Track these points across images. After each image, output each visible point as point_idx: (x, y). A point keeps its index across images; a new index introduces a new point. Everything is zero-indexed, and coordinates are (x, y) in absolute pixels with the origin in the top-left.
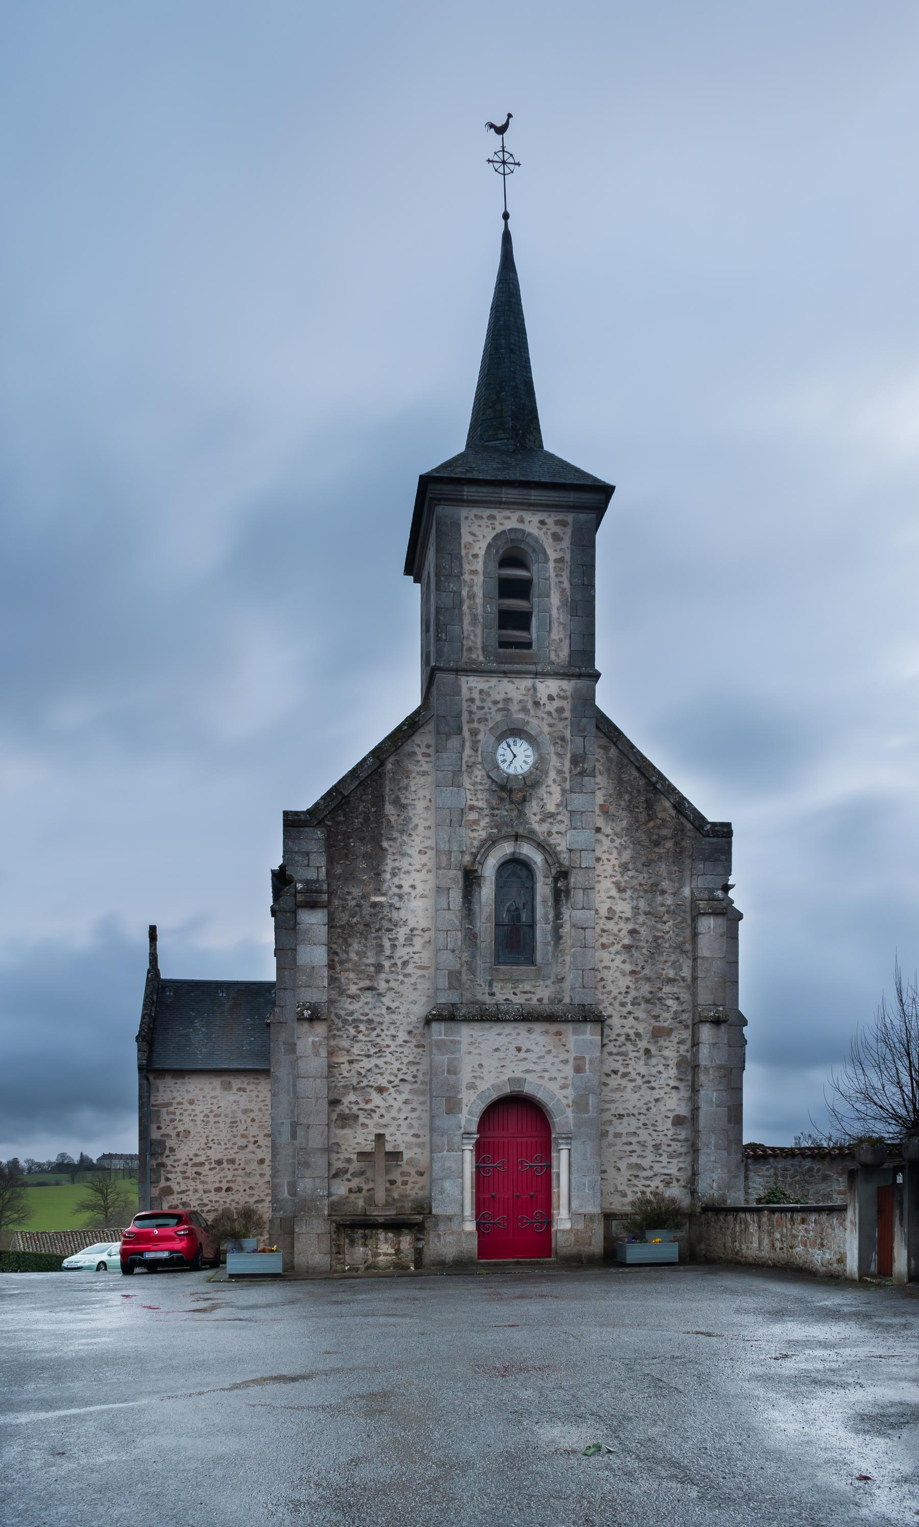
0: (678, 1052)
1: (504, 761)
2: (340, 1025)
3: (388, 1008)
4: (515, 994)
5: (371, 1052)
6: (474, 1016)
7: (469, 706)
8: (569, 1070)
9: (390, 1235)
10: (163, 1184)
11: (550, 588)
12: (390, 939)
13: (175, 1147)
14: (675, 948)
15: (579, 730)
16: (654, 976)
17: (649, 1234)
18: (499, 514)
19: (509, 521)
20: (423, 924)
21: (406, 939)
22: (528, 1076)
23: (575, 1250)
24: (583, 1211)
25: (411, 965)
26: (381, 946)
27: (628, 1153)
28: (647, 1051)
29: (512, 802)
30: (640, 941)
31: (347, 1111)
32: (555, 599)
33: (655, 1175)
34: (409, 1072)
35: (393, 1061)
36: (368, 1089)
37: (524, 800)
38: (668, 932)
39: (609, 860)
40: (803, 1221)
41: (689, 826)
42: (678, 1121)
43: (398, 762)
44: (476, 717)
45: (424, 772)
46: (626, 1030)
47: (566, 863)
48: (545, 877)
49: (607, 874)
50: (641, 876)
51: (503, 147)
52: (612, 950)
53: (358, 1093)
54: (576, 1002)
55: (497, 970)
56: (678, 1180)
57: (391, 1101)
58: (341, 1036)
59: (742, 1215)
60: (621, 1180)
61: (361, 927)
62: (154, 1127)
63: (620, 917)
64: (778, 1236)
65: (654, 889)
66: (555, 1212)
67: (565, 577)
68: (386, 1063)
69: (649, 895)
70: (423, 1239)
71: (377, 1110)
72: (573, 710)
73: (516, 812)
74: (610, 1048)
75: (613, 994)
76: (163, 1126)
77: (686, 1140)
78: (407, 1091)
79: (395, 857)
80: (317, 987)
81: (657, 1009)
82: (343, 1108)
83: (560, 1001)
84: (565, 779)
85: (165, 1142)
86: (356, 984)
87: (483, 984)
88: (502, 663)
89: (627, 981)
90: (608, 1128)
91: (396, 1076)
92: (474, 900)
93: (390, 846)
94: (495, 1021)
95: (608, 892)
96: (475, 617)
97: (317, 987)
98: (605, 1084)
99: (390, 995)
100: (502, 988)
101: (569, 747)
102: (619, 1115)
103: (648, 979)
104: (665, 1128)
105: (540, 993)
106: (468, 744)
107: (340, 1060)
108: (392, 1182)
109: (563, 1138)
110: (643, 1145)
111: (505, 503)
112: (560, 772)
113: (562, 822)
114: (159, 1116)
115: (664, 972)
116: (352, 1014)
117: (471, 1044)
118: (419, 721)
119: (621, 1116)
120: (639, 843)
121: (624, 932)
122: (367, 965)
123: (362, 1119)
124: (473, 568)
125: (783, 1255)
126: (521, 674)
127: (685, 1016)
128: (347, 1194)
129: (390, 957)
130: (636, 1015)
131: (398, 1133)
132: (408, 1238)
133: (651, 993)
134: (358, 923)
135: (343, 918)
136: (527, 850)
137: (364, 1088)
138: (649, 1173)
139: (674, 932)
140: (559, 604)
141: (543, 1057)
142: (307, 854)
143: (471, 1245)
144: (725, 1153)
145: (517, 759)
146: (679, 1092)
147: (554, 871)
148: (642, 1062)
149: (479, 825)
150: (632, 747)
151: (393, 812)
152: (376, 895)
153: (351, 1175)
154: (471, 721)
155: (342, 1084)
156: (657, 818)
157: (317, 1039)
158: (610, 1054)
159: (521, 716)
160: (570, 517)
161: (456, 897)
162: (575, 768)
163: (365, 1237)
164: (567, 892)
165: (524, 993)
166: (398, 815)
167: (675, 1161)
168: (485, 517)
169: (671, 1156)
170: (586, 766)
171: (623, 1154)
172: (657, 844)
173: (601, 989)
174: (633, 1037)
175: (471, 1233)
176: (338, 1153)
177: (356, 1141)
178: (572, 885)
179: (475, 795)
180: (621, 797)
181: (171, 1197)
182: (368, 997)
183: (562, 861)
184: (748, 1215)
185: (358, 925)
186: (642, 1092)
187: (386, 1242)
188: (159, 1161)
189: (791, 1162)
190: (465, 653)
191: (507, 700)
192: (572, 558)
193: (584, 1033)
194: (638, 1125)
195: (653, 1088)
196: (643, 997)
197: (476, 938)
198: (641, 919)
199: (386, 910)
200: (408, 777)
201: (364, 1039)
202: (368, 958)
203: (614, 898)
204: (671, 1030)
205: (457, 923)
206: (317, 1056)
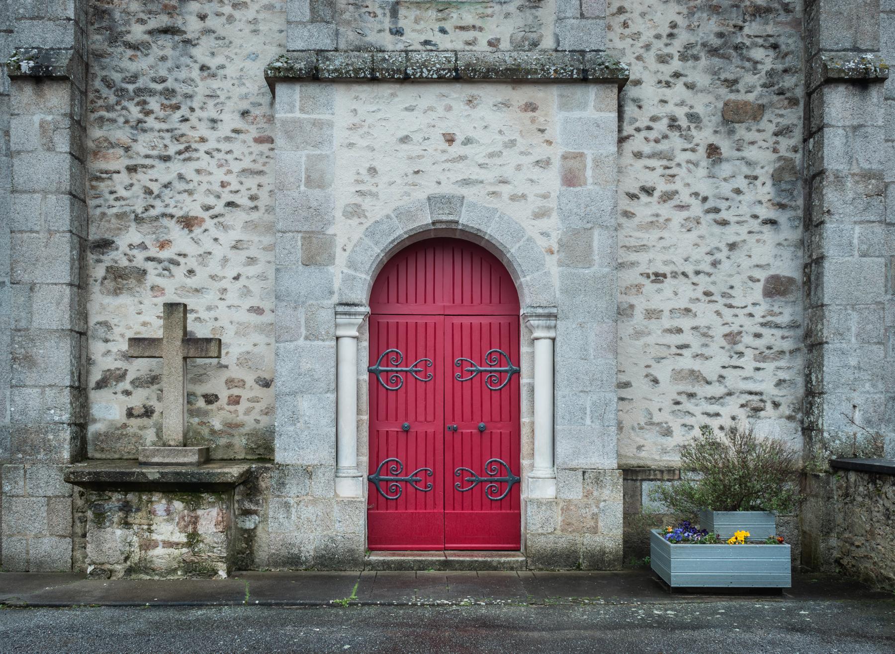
0: (775, 151)
2: (113, 99)
3: (203, 68)
4: (443, 31)
6: (357, 71)
8: (552, 180)
9: (178, 505)
17: (722, 522)
23: (563, 542)
24: (582, 462)
27: (674, 350)
28: (713, 150)
31: (124, 262)
33: (730, 394)
34: (243, 188)
36: (165, 221)
42: (776, 288)
46: (670, 108)
53: (146, 227)
56: (776, 405)
57: (207, 244)
58: (113, 121)
60: (659, 402)
66: (525, 462)
68: (198, 171)
70: (255, 512)
71: (181, 260)
74: (637, 143)
75: (644, 39)
77: (794, 326)
78: (239, 224)
82: (117, 257)
83: (535, 44)
86: (142, 21)
87: (379, 12)
90: (632, 299)
91: (218, 197)
99: (207, 43)
100: (417, 21)
102: (656, 275)
104: (749, 300)
107: (112, 166)
108: (211, 399)
109: (539, 316)
110: (705, 335)
116: (134, 78)
117: (354, 127)
119: (659, 277)
123: (152, 278)
127: (789, 81)
130: (689, 80)
131: (221, 304)
133: (720, 35)
137: (157, 218)
138: (717, 390)
141: (499, 154)
143: (352, 528)
146: (777, 231)
148: (702, 172)
153: (132, 382)
157: (49, 118)
158: (638, 155)
163: (126, 508)
165: (462, 28)
167: (770, 366)
169: (762, 357)
171: (664, 352)
173: (619, 30)
174: (683, 122)
175: (351, 502)
182: (165, 46)
186: (703, 229)
193: (583, 106)
194: (694, 295)
195: (724, 223)
196: (704, 45)
201: (158, 125)
204: (762, 108)
206: (49, 149)
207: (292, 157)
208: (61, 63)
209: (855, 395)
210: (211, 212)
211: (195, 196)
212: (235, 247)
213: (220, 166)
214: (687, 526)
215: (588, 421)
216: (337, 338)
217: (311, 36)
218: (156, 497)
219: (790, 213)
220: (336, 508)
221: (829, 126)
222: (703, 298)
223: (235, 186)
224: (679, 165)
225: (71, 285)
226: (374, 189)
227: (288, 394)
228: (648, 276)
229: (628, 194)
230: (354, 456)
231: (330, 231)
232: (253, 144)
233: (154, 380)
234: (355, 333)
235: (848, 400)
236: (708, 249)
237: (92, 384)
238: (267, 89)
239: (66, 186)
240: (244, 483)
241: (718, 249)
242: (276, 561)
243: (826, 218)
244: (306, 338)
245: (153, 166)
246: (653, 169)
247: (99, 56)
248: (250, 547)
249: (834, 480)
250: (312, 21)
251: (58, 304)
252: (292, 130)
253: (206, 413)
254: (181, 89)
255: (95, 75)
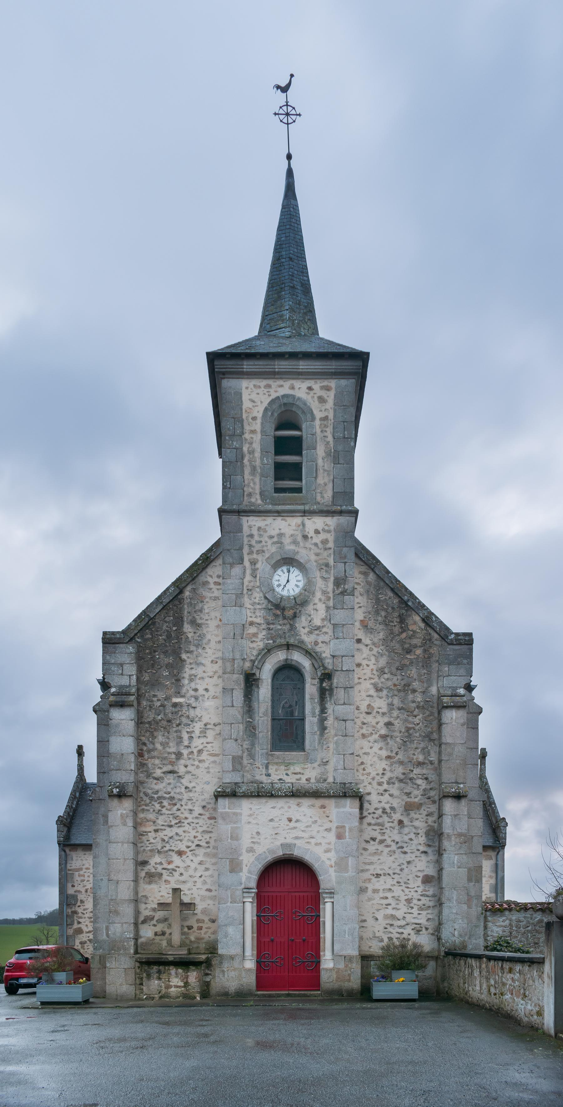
0: (426, 822)
1: (279, 586)
2: (148, 801)
3: (186, 788)
4: (287, 775)
5: (173, 823)
6: (251, 793)
7: (249, 541)
8: (332, 837)
9: (180, 971)
10: (76, 926)
11: (316, 441)
12: (188, 732)
13: (84, 899)
14: (424, 737)
15: (340, 558)
16: (406, 760)
17: (395, 974)
18: (274, 383)
19: (282, 388)
20: (216, 720)
21: (201, 732)
22: (298, 842)
23: (336, 986)
24: (344, 953)
25: (205, 753)
26: (181, 738)
27: (384, 906)
28: (401, 822)
29: (284, 618)
30: (394, 731)
31: (153, 870)
32: (321, 451)
33: (407, 924)
34: (203, 839)
35: (190, 830)
36: (170, 853)
37: (295, 616)
38: (418, 724)
39: (368, 666)
40: (510, 971)
41: (436, 636)
42: (427, 880)
43: (194, 590)
44: (254, 550)
45: (215, 597)
46: (383, 805)
47: (330, 667)
48: (313, 679)
49: (366, 677)
50: (395, 678)
51: (287, 102)
52: (372, 738)
53: (162, 856)
54: (338, 781)
55: (272, 755)
56: (427, 929)
57: (188, 862)
58: (148, 810)
59: (469, 960)
61: (164, 723)
62: (69, 885)
63: (378, 712)
64: (492, 982)
65: (406, 688)
66: (321, 953)
67: (329, 432)
68: (184, 832)
69: (402, 694)
70: (210, 974)
71: (177, 869)
72: (335, 541)
73: (288, 626)
74: (369, 819)
76: (76, 885)
77: (434, 896)
78: (202, 854)
79: (192, 666)
80: (126, 770)
81: (409, 788)
82: (150, 868)
83: (325, 780)
84: (329, 599)
85: (77, 896)
86: (160, 768)
87: (261, 767)
88: (276, 505)
89: (384, 764)
90: (367, 885)
91: (193, 842)
92: (253, 699)
93: (188, 657)
94: (269, 796)
95: (366, 692)
96: (254, 469)
97: (126, 770)
98: (365, 849)
99: (188, 777)
100: (276, 770)
101: (332, 571)
102: (377, 874)
103: (401, 763)
104: (416, 885)
105: (303, 772)
106: (248, 572)
107: (148, 829)
108: (190, 928)
109: (327, 893)
110: (397, 900)
111: (279, 373)
112: (324, 592)
113: (326, 633)
114: (73, 878)
115: (415, 757)
116: (157, 792)
117: (250, 815)
118: (211, 556)
119: (378, 876)
120: (393, 651)
121: (381, 724)
122: (169, 753)
123: (165, 877)
124: (252, 429)
125: (495, 1000)
126: (292, 513)
127: (432, 793)
128: (153, 937)
129: (188, 747)
130: (391, 792)
131: (194, 888)
132: (195, 973)
133: (404, 774)
134: (162, 719)
135: (150, 716)
136: (297, 657)
137: (167, 851)
138: (402, 923)
139: (423, 723)
140: (324, 454)
142: (122, 665)
143: (250, 980)
144: (465, 907)
145: (289, 583)
147: (319, 674)
148: (396, 831)
149: (257, 637)
150: (388, 572)
151: (190, 630)
152: (176, 697)
153: (157, 921)
154: (251, 553)
155: (149, 848)
156: (409, 630)
157: (124, 812)
158: (369, 824)
159: (292, 547)
160: (333, 383)
161: (239, 696)
162: (337, 589)
163: (159, 972)
164: (331, 690)
165: (295, 774)
166: (195, 633)
167: (424, 913)
168: (262, 386)
170: (346, 587)
171: (380, 907)
172: (409, 652)
173: (361, 771)
174: (388, 810)
175: (249, 970)
176: (146, 903)
177: (161, 894)
178: (335, 685)
179: (254, 613)
180: (378, 614)
181: (81, 935)
183: (326, 665)
184: (473, 960)
185: (162, 722)
186: (396, 855)
187: (177, 977)
188: (73, 910)
189: (524, 915)
190: (246, 498)
191: (281, 535)
192: (335, 416)
193: (344, 806)
195: (405, 853)
196: (397, 778)
197: (255, 729)
198: (395, 713)
199: (185, 709)
200: (202, 602)
201: (167, 812)
202: (170, 747)
203: (372, 696)
205: (240, 717)
206: (124, 825)
207: (225, 828)
208: (130, 789)
209: (455, 925)
210: (190, 849)
211: (183, 842)
212: (200, 864)
213: (194, 829)
214: (383, 977)
215: (347, 936)
216: (244, 902)
217: (233, 777)
218: (171, 967)
219: (432, 849)
220: (243, 973)
221: (445, 814)
222: (396, 884)
223: (200, 838)
224: (386, 828)
225: (133, 881)
226: (259, 841)
227: (224, 926)
228: (374, 875)
229: (365, 841)
230: (250, 951)
231: (241, 858)
232: (207, 820)
233: (166, 920)
234: (251, 900)
235: (452, 927)
236: (398, 864)
237: (140, 922)
238: (214, 800)
239: (131, 840)
240: (206, 962)
241: (403, 864)
242: (219, 994)
243: (444, 852)
244: (231, 902)
245: (165, 830)
246: (376, 830)
247: (142, 783)
248: (208, 989)
249: (446, 959)
250: (233, 771)
251: (128, 889)
252: (225, 817)
253: (188, 934)
254: (177, 796)
255: (140, 791)
